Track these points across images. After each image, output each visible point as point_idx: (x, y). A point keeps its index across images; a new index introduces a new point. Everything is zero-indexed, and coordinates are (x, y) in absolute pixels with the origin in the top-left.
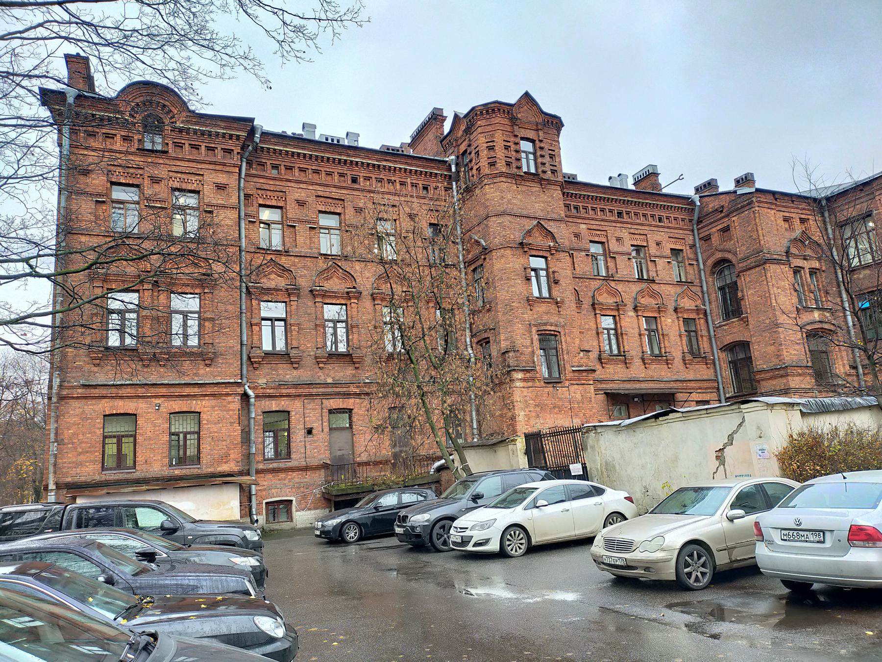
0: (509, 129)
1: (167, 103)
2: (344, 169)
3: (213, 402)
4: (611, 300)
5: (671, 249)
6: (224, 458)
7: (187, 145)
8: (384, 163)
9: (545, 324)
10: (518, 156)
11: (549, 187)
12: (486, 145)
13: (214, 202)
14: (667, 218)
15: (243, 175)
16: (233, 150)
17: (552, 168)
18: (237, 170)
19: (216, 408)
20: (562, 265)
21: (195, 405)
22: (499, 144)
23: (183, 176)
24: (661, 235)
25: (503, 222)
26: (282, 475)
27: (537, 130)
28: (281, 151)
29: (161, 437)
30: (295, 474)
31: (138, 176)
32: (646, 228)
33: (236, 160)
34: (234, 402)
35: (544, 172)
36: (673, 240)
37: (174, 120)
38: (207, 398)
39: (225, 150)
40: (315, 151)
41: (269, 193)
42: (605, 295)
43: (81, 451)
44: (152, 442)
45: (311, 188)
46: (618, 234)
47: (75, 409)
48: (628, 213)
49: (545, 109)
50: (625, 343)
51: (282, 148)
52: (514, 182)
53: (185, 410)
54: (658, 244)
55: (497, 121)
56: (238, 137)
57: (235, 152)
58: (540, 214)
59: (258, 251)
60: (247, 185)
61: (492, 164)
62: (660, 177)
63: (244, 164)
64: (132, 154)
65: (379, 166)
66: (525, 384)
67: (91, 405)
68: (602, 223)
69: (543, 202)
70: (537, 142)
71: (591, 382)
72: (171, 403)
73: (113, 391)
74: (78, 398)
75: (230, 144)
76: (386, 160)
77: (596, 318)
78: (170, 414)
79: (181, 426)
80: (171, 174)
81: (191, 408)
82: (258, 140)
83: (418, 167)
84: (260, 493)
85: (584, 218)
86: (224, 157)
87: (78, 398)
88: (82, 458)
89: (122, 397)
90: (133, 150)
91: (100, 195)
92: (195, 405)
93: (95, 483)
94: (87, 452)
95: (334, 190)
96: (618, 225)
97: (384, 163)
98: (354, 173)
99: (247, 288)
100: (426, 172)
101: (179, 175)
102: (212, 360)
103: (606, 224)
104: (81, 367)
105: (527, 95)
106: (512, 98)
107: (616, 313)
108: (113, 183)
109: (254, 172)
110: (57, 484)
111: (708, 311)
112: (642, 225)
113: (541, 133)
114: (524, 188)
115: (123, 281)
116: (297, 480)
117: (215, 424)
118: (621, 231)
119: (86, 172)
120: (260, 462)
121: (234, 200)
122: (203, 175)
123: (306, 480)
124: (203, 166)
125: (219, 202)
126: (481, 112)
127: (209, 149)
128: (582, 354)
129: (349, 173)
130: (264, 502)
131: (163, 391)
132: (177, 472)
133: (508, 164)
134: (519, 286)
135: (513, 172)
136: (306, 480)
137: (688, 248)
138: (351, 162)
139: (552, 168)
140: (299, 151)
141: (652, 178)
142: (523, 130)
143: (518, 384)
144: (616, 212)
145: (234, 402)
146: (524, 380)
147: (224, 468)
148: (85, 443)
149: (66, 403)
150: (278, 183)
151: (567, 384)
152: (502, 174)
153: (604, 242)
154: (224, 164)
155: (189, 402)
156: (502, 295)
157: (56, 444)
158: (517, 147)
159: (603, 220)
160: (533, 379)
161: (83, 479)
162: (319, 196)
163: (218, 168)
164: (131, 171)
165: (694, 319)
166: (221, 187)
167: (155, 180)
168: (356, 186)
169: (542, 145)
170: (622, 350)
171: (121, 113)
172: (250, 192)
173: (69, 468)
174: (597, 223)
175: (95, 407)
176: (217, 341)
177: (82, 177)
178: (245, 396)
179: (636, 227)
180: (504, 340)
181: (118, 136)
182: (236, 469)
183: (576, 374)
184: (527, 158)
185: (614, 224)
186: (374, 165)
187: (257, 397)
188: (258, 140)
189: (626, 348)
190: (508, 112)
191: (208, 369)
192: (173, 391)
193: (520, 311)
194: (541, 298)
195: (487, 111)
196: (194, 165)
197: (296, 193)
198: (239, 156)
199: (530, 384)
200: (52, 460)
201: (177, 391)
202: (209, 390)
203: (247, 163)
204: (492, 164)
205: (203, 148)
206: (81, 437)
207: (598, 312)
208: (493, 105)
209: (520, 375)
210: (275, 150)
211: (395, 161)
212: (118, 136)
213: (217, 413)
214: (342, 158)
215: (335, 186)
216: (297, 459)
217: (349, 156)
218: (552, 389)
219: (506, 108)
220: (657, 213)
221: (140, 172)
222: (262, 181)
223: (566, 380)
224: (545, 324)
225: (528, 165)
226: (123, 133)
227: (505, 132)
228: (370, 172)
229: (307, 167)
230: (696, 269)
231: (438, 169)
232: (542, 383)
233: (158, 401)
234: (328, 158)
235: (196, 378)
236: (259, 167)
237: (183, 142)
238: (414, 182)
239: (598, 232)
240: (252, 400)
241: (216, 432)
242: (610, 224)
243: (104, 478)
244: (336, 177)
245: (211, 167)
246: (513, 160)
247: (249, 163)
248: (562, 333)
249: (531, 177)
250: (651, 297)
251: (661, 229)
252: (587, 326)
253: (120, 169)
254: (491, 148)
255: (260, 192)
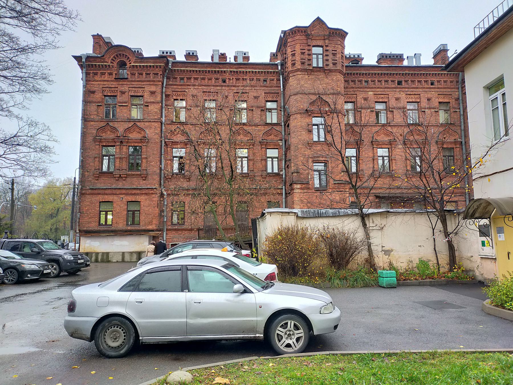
0: (305, 42)
1: (127, 54)
2: (218, 76)
3: (146, 197)
4: (386, 139)
5: (439, 102)
6: (150, 223)
7: (137, 74)
8: (240, 70)
9: (318, 157)
10: (310, 57)
11: (330, 74)
12: (291, 53)
13: (149, 101)
14: (438, 82)
15: (164, 86)
16: (158, 73)
17: (333, 62)
18: (160, 83)
19: (147, 200)
20: (334, 122)
21: (138, 198)
22: (298, 51)
23: (135, 89)
24: (433, 94)
25: (297, 99)
26: (180, 232)
27: (325, 40)
28: (184, 70)
29: (123, 212)
30: (186, 232)
31: (116, 91)
32: (420, 90)
33: (160, 78)
34: (156, 197)
35: (327, 65)
36: (442, 96)
37: (130, 62)
38: (143, 195)
39: (155, 74)
40: (202, 68)
41: (179, 93)
42: (383, 135)
43: (90, 217)
44: (119, 214)
45: (200, 88)
46: (397, 95)
47: (88, 199)
48: (406, 81)
49: (330, 26)
50: (394, 165)
51: (184, 69)
52: (306, 73)
53: (134, 200)
54: (429, 100)
55: (297, 38)
56: (160, 66)
57: (159, 74)
58: (321, 91)
59: (172, 123)
60: (167, 90)
61: (293, 64)
62: (448, 52)
63: (165, 80)
64: (112, 81)
65: (237, 72)
66: (302, 191)
67: (95, 197)
68: (386, 90)
69: (326, 83)
70: (324, 47)
71: (347, 190)
72: (128, 197)
73: (103, 191)
74: (89, 194)
75: (157, 71)
76: (241, 68)
77: (373, 150)
78: (128, 202)
79: (132, 208)
80: (130, 89)
81: (136, 199)
82: (170, 67)
83: (260, 69)
84: (168, 240)
85: (372, 88)
86: (154, 78)
87: (89, 194)
88: (90, 220)
89: (107, 194)
90: (113, 79)
91: (99, 102)
92: (138, 198)
93: (95, 231)
94: (93, 218)
95: (212, 87)
96: (398, 90)
97: (240, 70)
98: (223, 77)
99: (165, 142)
100: (265, 72)
101: (134, 89)
102: (146, 177)
103: (389, 90)
104: (90, 181)
105: (318, 19)
106: (306, 23)
107: (390, 147)
108: (105, 96)
109: (171, 83)
110: (79, 230)
111: (463, 143)
112: (417, 88)
113: (327, 41)
114: (313, 77)
115: (108, 142)
116: (186, 235)
117: (147, 207)
118: (400, 94)
119: (93, 92)
120: (170, 226)
121: (159, 99)
122: (144, 88)
123: (191, 235)
124: (144, 83)
125: (152, 100)
126: (289, 34)
127: (147, 74)
128: (343, 173)
129: (220, 77)
130: (170, 244)
131: (124, 191)
132: (129, 228)
133: (303, 63)
134: (304, 136)
135: (305, 68)
136: (191, 235)
137: (454, 100)
138: (222, 71)
139: (333, 62)
140: (193, 69)
141: (442, 54)
142: (315, 41)
143: (297, 191)
144: (397, 81)
145: (156, 197)
146: (301, 189)
147: (150, 227)
148: (92, 213)
149: (85, 196)
150: (183, 87)
151: (330, 190)
152: (298, 70)
153: (386, 102)
154: (154, 81)
155: (135, 197)
156: (294, 141)
157: (79, 214)
158: (310, 52)
159: (386, 88)
160: (309, 188)
161: (91, 229)
162: (204, 92)
163: (151, 83)
164: (113, 89)
165: (453, 148)
166: (153, 93)
167: (123, 93)
168: (224, 84)
169: (328, 48)
170: (391, 169)
171: (107, 63)
172: (169, 93)
173: (86, 224)
174: (382, 90)
175: (96, 198)
176: (149, 168)
177: (92, 95)
178: (162, 195)
179: (411, 90)
180: (293, 166)
181: (107, 73)
182: (155, 228)
183: (337, 185)
184: (317, 58)
185: (394, 90)
186: (234, 71)
187: (168, 195)
188: (170, 67)
189: (394, 168)
190: (305, 31)
191: (144, 182)
192: (128, 191)
193: (303, 150)
194: (319, 142)
195: (292, 33)
196: (140, 83)
197: (192, 91)
198: (162, 76)
199: (306, 191)
200: (78, 221)
201: (130, 192)
202: (144, 192)
203: (167, 78)
204: (293, 64)
205: (144, 74)
206: (90, 211)
207: (374, 146)
208: (294, 29)
209: (299, 186)
210: (181, 70)
211: (246, 68)
212: (107, 73)
213: (148, 202)
214: (216, 70)
215: (213, 86)
216: (187, 226)
217: (220, 68)
218: (319, 194)
219: (303, 29)
220: (430, 79)
221: (116, 89)
222: (175, 87)
223: (330, 189)
224: (318, 157)
225: (317, 62)
226: (109, 72)
227: (301, 44)
228: (232, 75)
229: (198, 77)
230: (458, 114)
231: (272, 69)
232: (313, 190)
233: (122, 196)
234: (209, 71)
235: (139, 186)
236: (174, 80)
237: (135, 72)
238: (258, 78)
239: (382, 96)
240: (165, 197)
241: (147, 211)
242: (391, 90)
243: (99, 229)
244: (206, 80)
245: (148, 83)
246: (306, 61)
247: (168, 78)
248: (330, 162)
249: (318, 69)
250: (418, 135)
251: (432, 90)
252: (366, 155)
253: (108, 89)
254: (293, 55)
255: (174, 93)
